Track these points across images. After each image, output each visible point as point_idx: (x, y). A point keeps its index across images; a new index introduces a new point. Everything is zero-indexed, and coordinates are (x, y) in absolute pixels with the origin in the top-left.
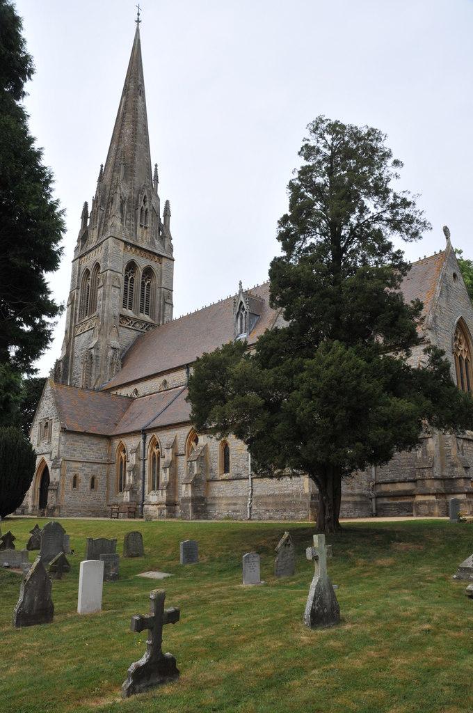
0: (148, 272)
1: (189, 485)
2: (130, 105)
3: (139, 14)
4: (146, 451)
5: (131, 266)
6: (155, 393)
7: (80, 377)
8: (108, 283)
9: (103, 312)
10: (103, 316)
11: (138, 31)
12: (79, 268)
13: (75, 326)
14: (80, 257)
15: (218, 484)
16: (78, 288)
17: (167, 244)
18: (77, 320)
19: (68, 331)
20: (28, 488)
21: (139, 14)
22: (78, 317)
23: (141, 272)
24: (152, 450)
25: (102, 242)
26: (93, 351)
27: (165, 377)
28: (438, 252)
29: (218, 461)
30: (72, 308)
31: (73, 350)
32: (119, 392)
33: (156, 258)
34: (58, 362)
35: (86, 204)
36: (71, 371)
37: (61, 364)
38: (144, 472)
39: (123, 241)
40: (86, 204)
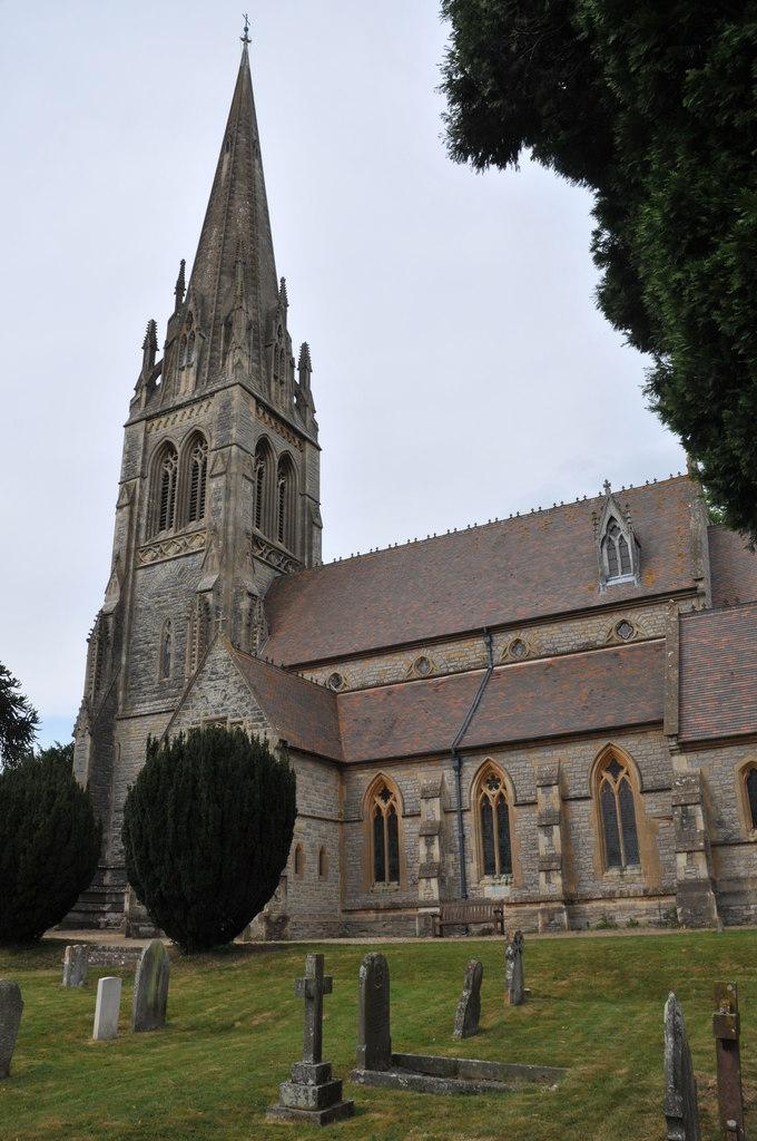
0: (286, 461)
1: (700, 856)
2: (242, 169)
3: (246, 29)
4: (465, 793)
5: (263, 446)
6: (402, 682)
7: (155, 649)
8: (234, 469)
9: (226, 523)
10: (226, 531)
11: (245, 55)
12: (145, 438)
13: (137, 549)
14: (148, 419)
15: (745, 850)
16: (143, 477)
17: (309, 418)
18: (142, 536)
19: (123, 557)
20: (283, 865)
21: (246, 29)
22: (143, 528)
23: (277, 460)
24: (479, 791)
25: (212, 394)
26: (210, 596)
27: (425, 652)
28: (452, 531)
29: (740, 805)
30: (131, 513)
31: (133, 594)
32: (308, 675)
33: (297, 440)
34: (103, 616)
35: (152, 326)
36: (130, 635)
37: (111, 620)
38: (463, 838)
39: (255, 397)
40: (152, 326)
